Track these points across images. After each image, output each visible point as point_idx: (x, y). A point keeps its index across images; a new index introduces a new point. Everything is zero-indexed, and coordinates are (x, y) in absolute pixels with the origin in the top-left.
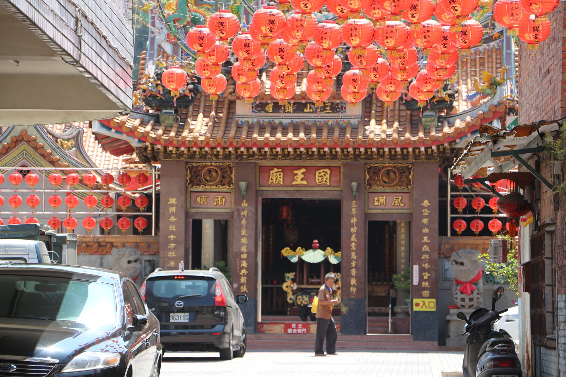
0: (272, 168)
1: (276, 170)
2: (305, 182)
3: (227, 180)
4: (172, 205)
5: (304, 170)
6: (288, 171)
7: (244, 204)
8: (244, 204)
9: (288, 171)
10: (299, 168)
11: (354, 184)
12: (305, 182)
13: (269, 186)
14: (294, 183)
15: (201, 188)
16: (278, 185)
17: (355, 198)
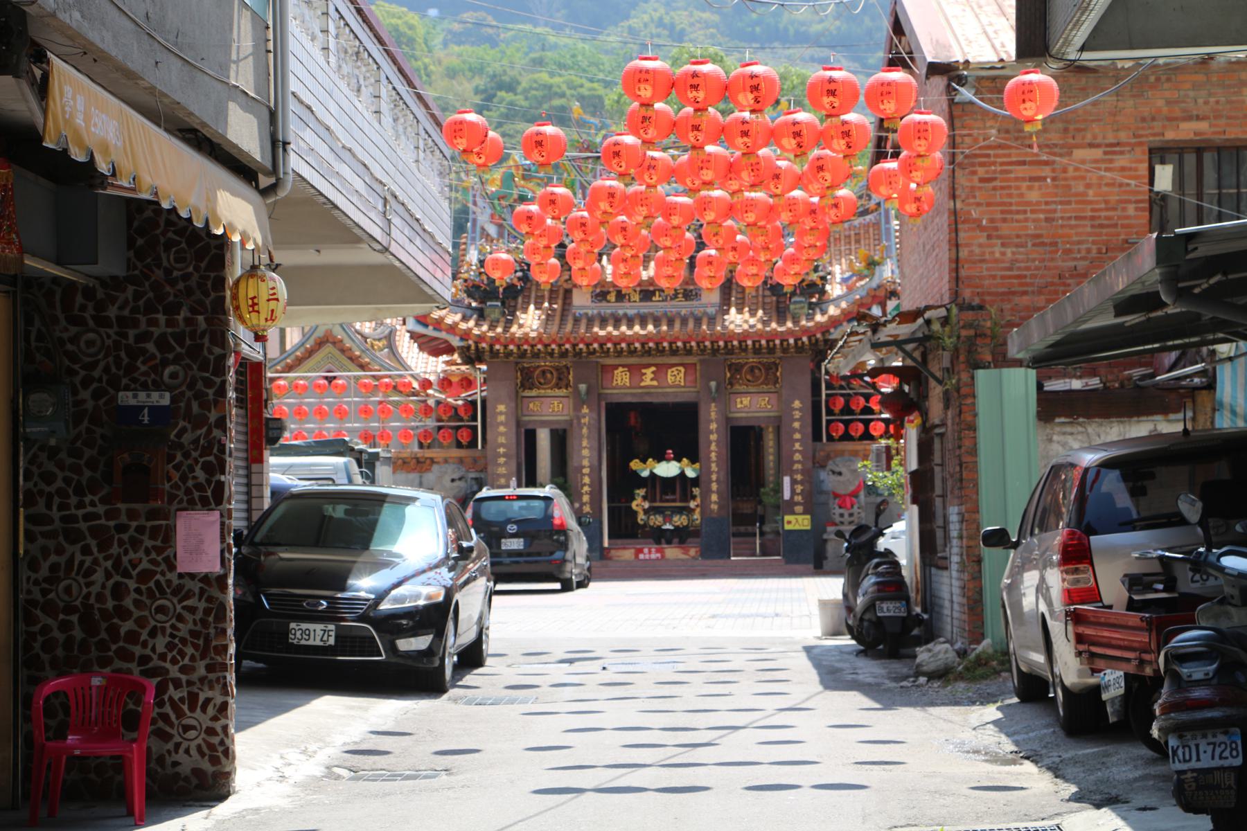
0: (616, 367)
1: (621, 369)
2: (655, 383)
3: (564, 383)
4: (501, 413)
5: (653, 369)
6: (635, 370)
7: (585, 410)
8: (585, 410)
9: (635, 370)
10: (648, 366)
11: (713, 384)
12: (655, 383)
13: (614, 388)
14: (643, 384)
15: (534, 393)
16: (624, 387)
17: (714, 400)
